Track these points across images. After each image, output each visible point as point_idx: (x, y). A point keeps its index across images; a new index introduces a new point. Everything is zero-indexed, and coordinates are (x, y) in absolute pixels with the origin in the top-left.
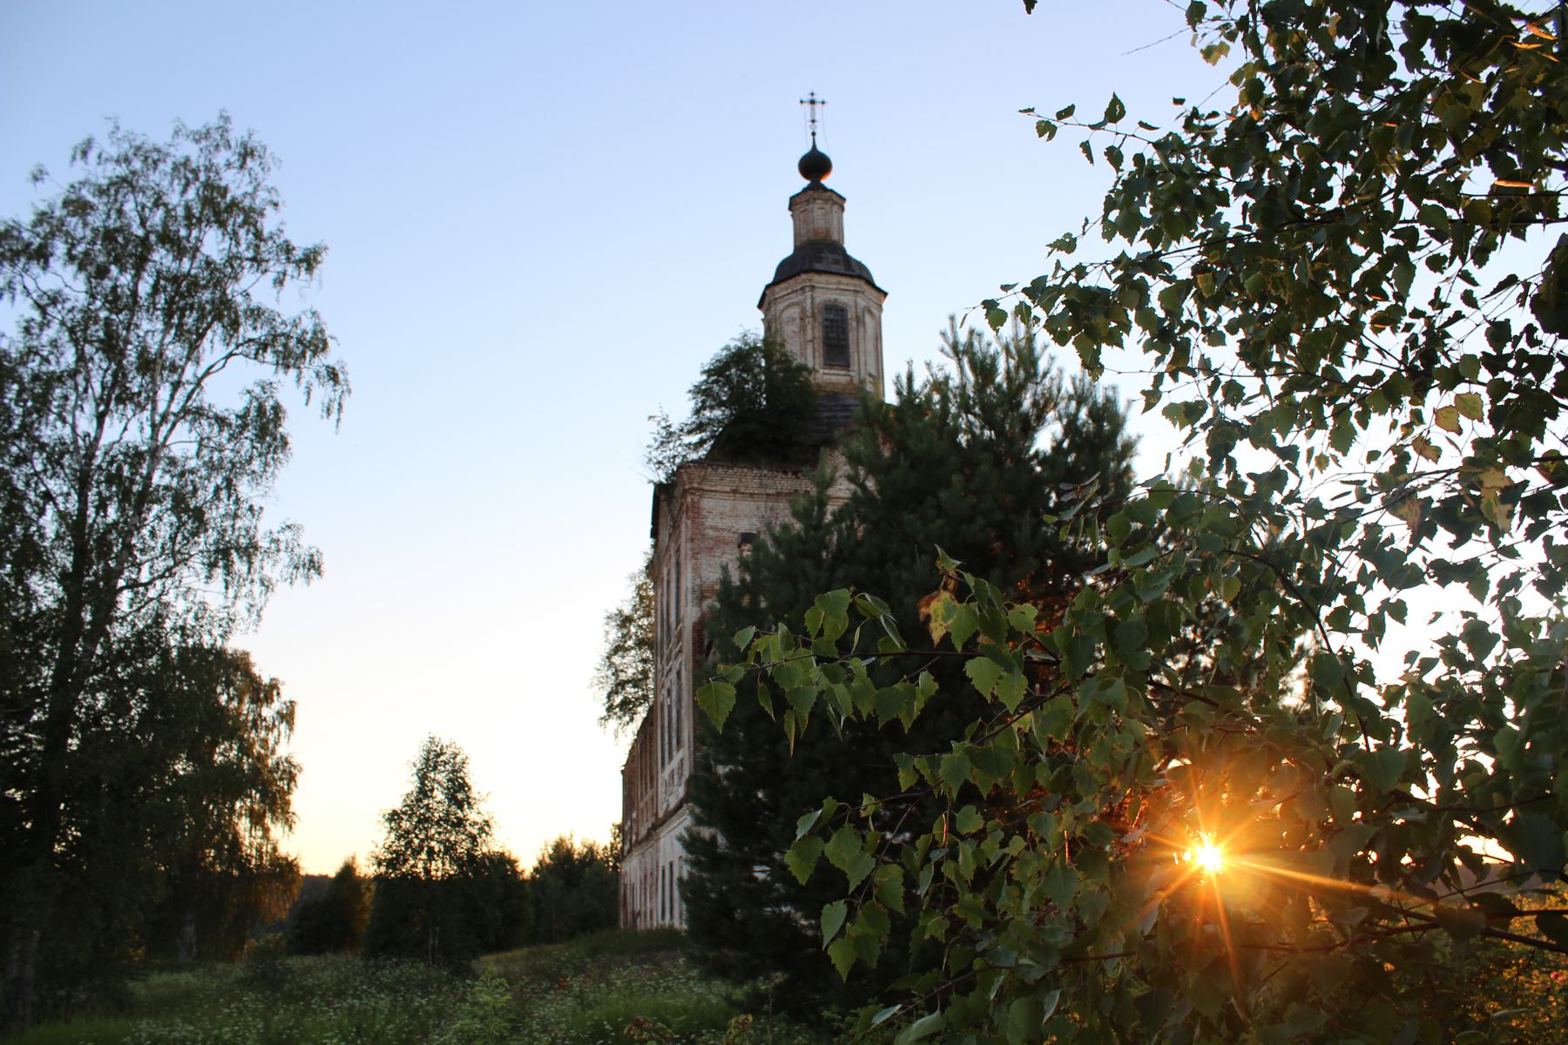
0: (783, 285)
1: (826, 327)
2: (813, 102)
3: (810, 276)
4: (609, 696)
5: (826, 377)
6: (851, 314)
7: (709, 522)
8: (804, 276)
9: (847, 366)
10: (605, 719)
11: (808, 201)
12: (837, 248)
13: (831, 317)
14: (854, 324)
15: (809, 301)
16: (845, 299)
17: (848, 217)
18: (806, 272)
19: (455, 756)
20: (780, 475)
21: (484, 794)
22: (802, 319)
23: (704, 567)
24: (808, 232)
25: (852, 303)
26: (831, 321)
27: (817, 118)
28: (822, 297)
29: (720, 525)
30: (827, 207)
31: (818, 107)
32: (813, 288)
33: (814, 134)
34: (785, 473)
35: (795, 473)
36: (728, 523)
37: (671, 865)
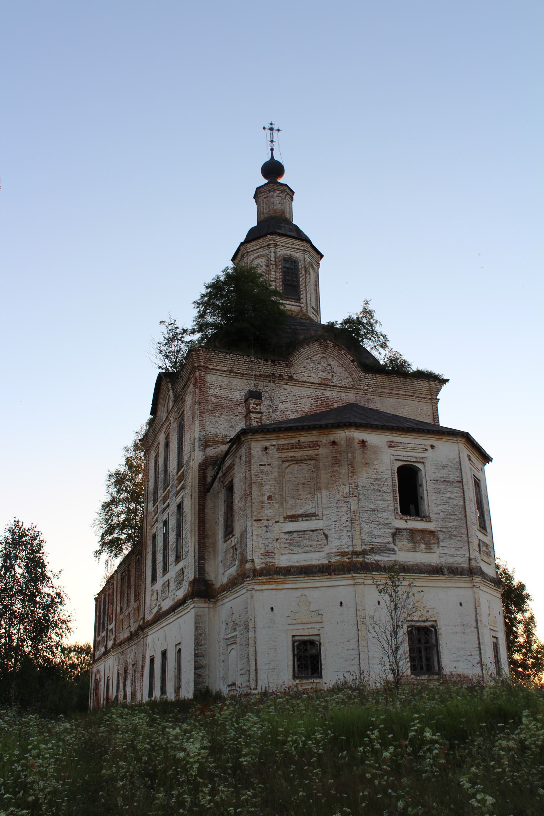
0: (253, 243)
1: (285, 272)
2: (272, 129)
3: (274, 237)
4: (103, 536)
5: (289, 306)
6: (301, 265)
7: (211, 391)
8: (269, 237)
9: (298, 300)
10: (99, 552)
11: (269, 191)
12: (289, 222)
13: (288, 266)
14: (303, 272)
15: (273, 254)
16: (297, 255)
17: (296, 204)
18: (271, 234)
19: (34, 538)
20: (263, 362)
21: (56, 572)
22: (267, 266)
23: (208, 423)
24: (270, 211)
25: (302, 259)
26: (288, 268)
27: (274, 140)
28: (282, 252)
29: (219, 394)
30: (283, 196)
31: (275, 133)
32: (276, 245)
33: (272, 150)
34: (267, 360)
35: (273, 362)
36: (224, 393)
37: (164, 654)
